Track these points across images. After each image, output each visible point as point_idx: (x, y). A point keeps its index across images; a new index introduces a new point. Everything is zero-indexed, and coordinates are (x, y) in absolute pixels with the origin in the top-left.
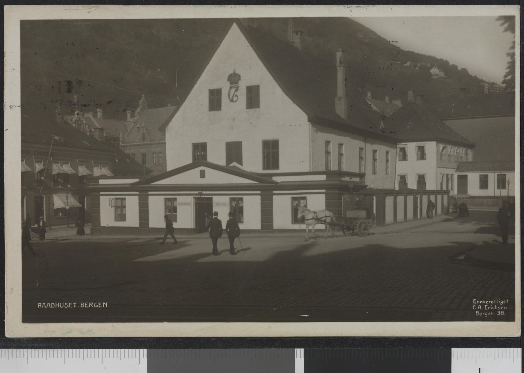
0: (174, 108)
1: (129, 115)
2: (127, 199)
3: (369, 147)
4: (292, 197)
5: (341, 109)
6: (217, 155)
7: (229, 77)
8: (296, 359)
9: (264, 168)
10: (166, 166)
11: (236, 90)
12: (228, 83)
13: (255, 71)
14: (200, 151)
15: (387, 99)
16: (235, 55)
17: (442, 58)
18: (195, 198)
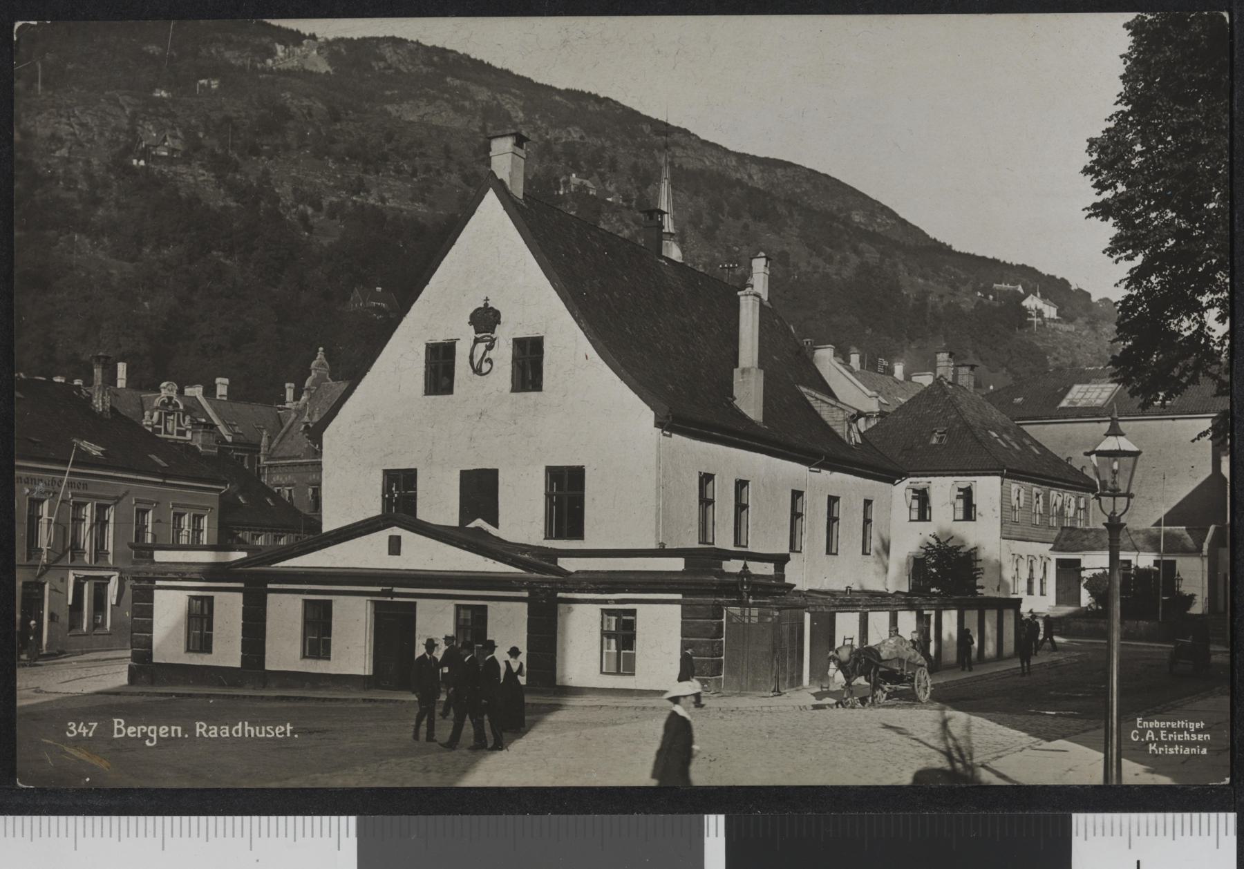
0: (343, 386)
1: (290, 394)
2: (215, 601)
4: (305, 601)
5: (749, 396)
6: (440, 502)
7: (472, 316)
9: (548, 536)
10: (320, 523)
11: (489, 348)
13: (534, 302)
14: (400, 489)
16: (492, 263)
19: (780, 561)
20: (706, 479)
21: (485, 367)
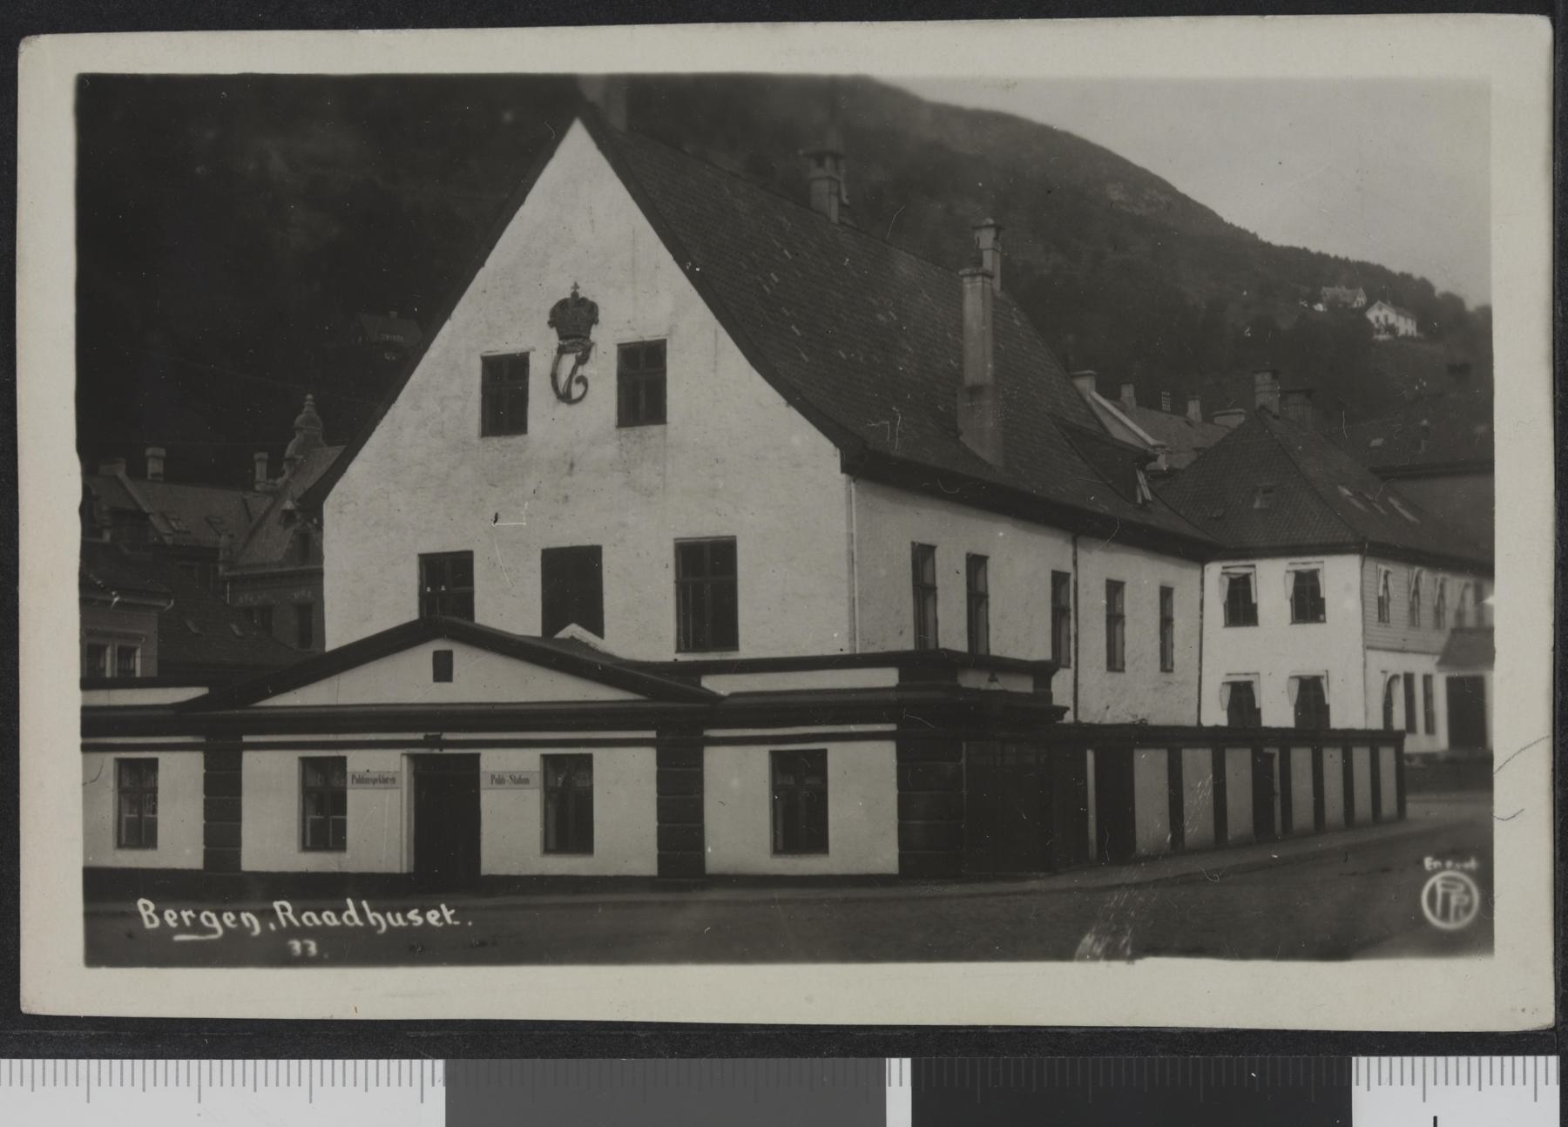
1: (261, 470)
3: (1097, 567)
6: (509, 599)
7: (553, 313)
8: (888, 1088)
11: (582, 360)
12: (553, 333)
13: (649, 293)
15: (1194, 408)
16: (580, 226)
17: (1406, 270)
18: (411, 757)
19: (1042, 672)
20: (923, 555)
21: (577, 390)
